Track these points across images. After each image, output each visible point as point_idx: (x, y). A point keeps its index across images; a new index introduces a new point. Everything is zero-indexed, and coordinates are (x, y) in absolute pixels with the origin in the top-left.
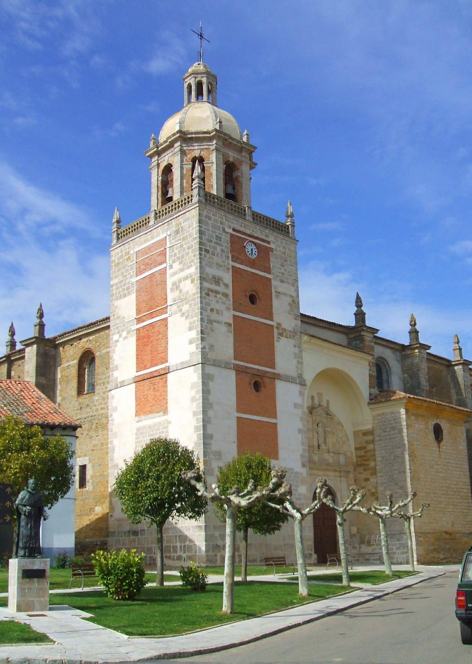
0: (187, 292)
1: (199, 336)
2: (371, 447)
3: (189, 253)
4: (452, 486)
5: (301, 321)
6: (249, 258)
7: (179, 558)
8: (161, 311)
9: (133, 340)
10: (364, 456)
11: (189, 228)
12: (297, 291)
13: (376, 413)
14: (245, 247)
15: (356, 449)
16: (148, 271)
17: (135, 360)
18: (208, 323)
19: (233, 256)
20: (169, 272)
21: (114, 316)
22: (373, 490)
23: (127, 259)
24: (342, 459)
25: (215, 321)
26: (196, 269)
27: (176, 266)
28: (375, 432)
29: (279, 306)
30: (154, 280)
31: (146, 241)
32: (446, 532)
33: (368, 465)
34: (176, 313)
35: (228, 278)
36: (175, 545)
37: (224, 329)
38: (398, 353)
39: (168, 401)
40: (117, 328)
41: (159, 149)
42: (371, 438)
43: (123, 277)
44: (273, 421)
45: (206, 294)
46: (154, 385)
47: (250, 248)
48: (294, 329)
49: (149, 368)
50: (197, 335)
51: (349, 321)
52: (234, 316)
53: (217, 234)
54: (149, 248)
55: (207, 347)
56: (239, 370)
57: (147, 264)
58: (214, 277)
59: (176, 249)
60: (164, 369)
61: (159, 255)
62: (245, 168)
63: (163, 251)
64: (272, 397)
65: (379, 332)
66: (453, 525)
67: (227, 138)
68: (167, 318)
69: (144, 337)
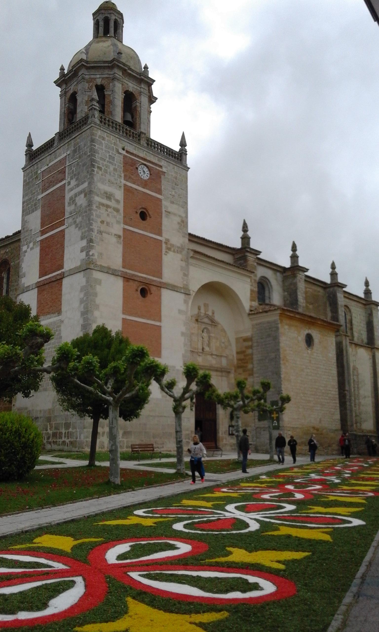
0: (81, 206)
2: (249, 351)
4: (322, 388)
5: (189, 240)
6: (141, 179)
9: (37, 250)
11: (84, 147)
12: (186, 212)
14: (137, 168)
15: (238, 353)
16: (51, 188)
18: (97, 233)
19: (125, 176)
20: (67, 188)
27: (73, 183)
28: (253, 339)
29: (169, 225)
32: (314, 428)
33: (246, 367)
35: (119, 194)
36: (61, 431)
37: (114, 240)
38: (278, 274)
40: (26, 240)
41: (66, 78)
42: (250, 343)
43: (32, 195)
44: (158, 324)
45: (96, 207)
48: (182, 245)
52: (124, 229)
53: (111, 154)
56: (127, 279)
60: (60, 274)
62: (144, 100)
65: (261, 254)
66: (320, 421)
67: (127, 69)
68: (64, 229)
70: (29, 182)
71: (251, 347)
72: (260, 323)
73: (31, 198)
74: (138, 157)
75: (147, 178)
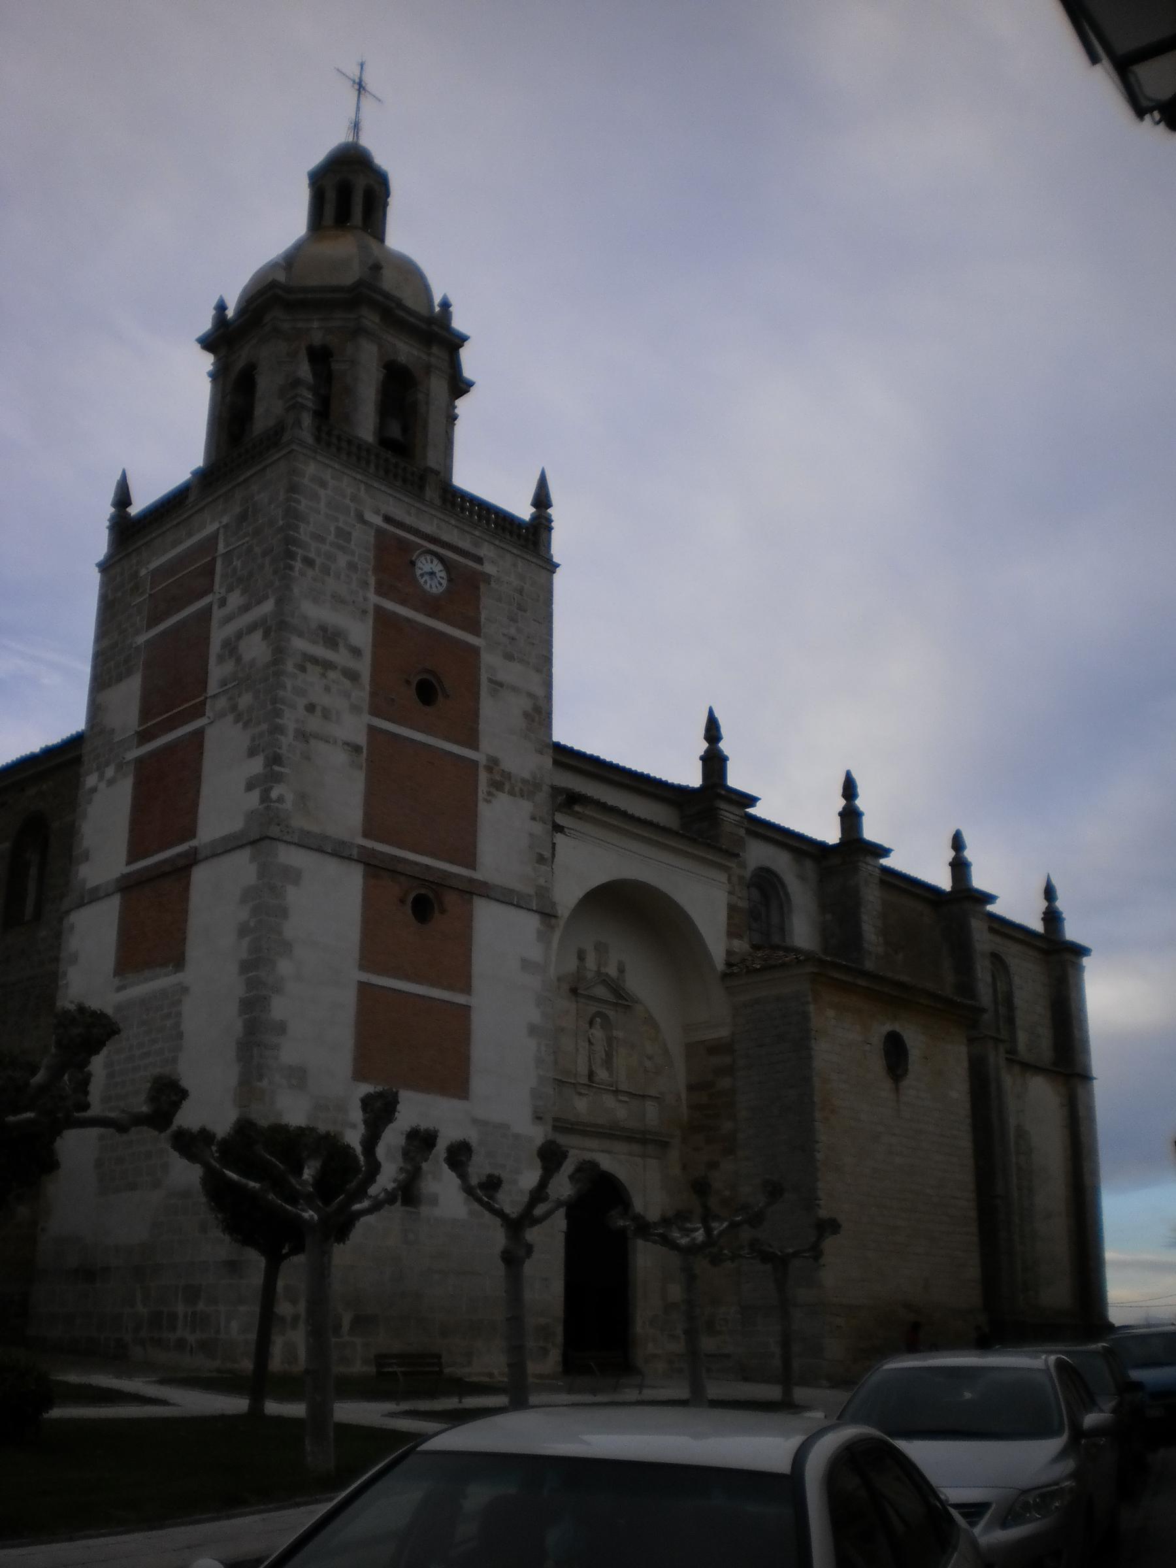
2: (725, 1083)
7: (181, 1344)
9: (125, 788)
14: (413, 563)
15: (691, 1088)
20: (218, 614)
22: (727, 1193)
24: (652, 1112)
25: (317, 736)
29: (496, 717)
31: (174, 545)
34: (222, 715)
35: (361, 633)
37: (340, 757)
38: (809, 865)
44: (460, 999)
47: (426, 565)
51: (691, 776)
53: (341, 525)
56: (376, 869)
58: (323, 629)
64: (464, 938)
74: (416, 532)
75: (441, 589)
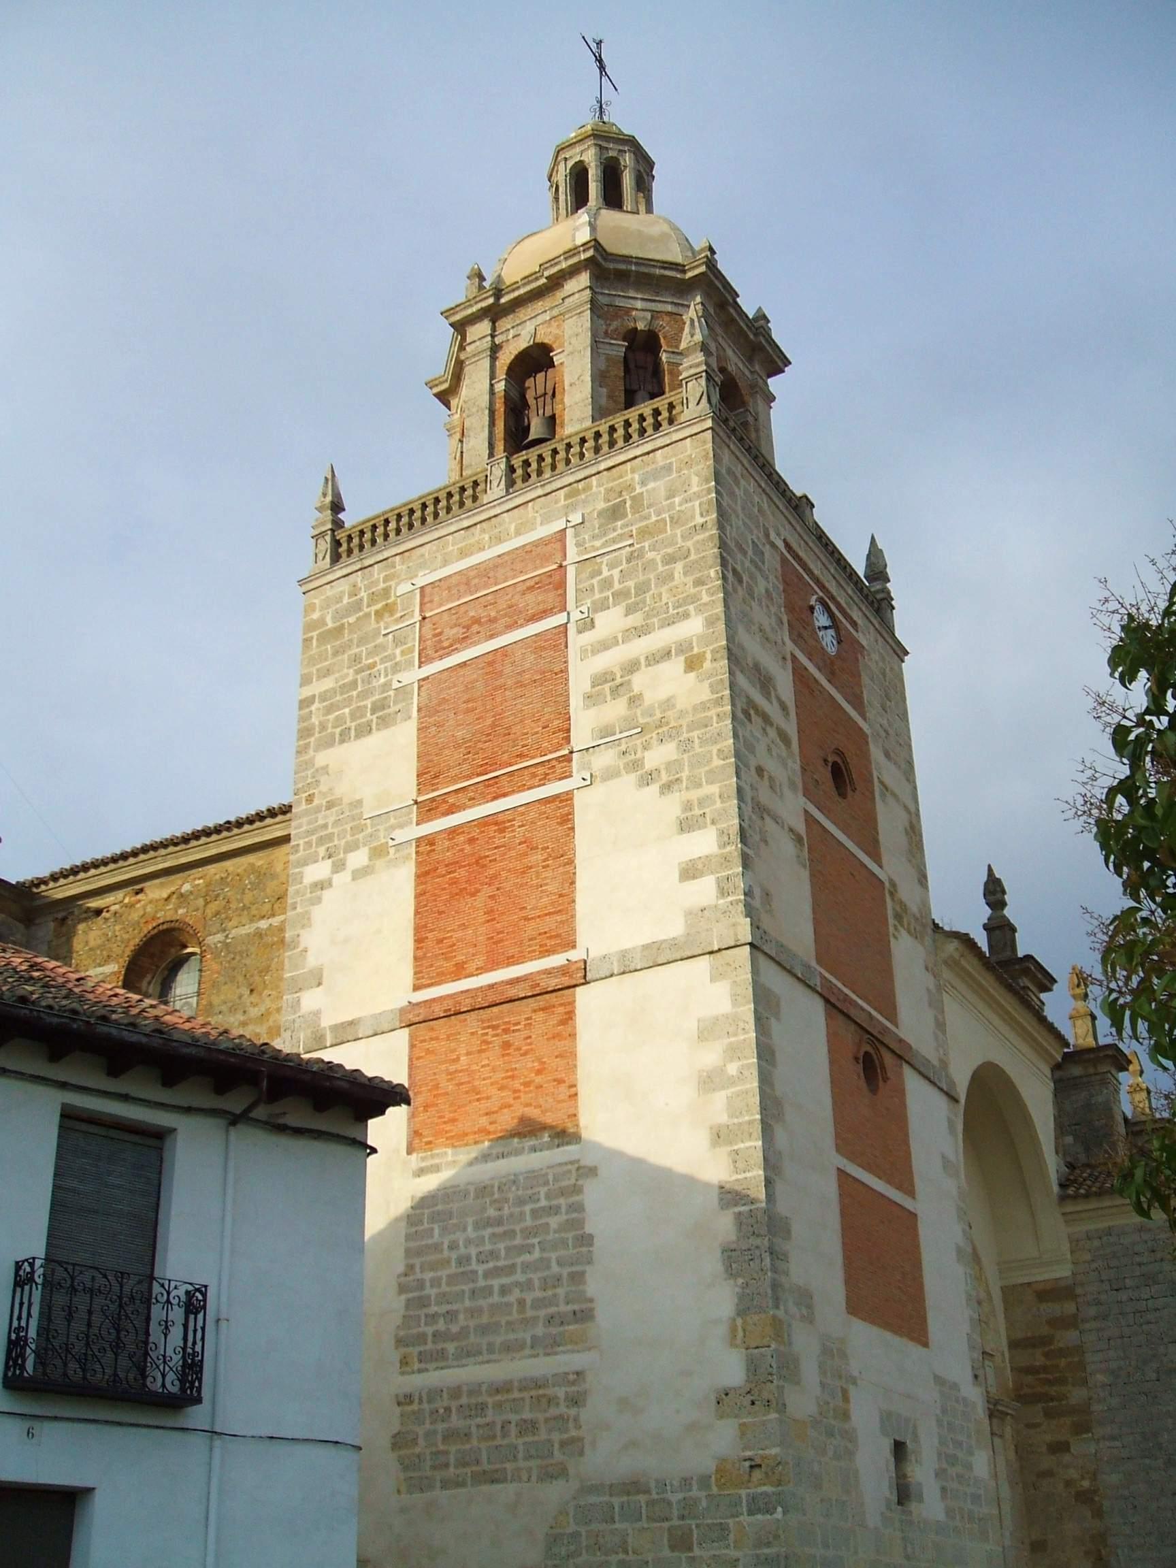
0: (668, 703)
1: (734, 849)
2: (1069, 1337)
3: (671, 577)
8: (541, 770)
9: (397, 887)
10: (1045, 1369)
13: (1081, 1228)
15: (1014, 1345)
17: (410, 944)
20: (576, 641)
21: (310, 799)
22: (1086, 1484)
23: (377, 612)
26: (710, 622)
28: (1079, 1291)
30: (508, 670)
31: (463, 553)
34: (610, 774)
39: (583, 1090)
42: (1069, 1308)
43: (357, 672)
46: (506, 1031)
49: (481, 970)
50: (723, 845)
54: (486, 572)
55: (757, 892)
57: (477, 621)
58: (757, 667)
59: (611, 566)
60: (564, 970)
61: (531, 588)
63: (549, 574)
69: (453, 865)
70: (339, 630)
71: (1070, 1322)
72: (1109, 1232)
73: (355, 683)
